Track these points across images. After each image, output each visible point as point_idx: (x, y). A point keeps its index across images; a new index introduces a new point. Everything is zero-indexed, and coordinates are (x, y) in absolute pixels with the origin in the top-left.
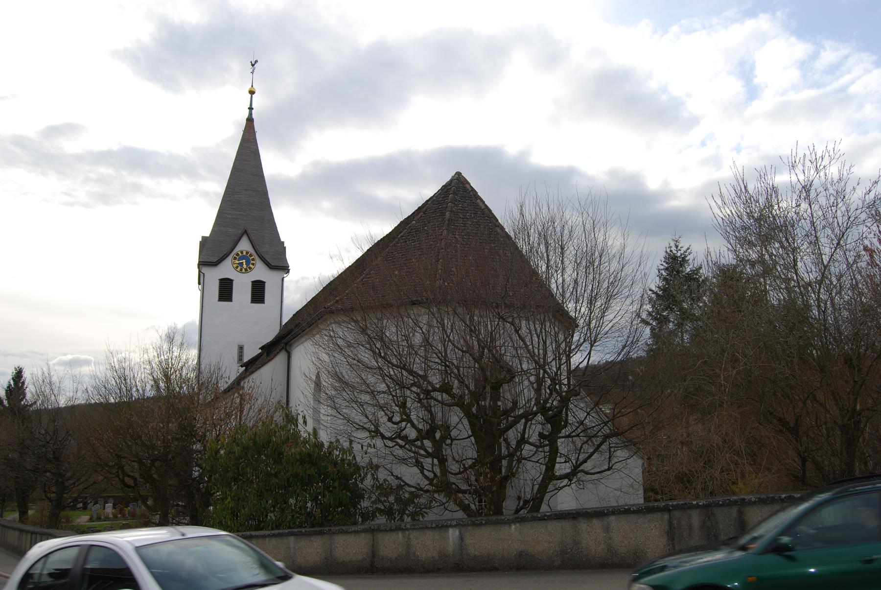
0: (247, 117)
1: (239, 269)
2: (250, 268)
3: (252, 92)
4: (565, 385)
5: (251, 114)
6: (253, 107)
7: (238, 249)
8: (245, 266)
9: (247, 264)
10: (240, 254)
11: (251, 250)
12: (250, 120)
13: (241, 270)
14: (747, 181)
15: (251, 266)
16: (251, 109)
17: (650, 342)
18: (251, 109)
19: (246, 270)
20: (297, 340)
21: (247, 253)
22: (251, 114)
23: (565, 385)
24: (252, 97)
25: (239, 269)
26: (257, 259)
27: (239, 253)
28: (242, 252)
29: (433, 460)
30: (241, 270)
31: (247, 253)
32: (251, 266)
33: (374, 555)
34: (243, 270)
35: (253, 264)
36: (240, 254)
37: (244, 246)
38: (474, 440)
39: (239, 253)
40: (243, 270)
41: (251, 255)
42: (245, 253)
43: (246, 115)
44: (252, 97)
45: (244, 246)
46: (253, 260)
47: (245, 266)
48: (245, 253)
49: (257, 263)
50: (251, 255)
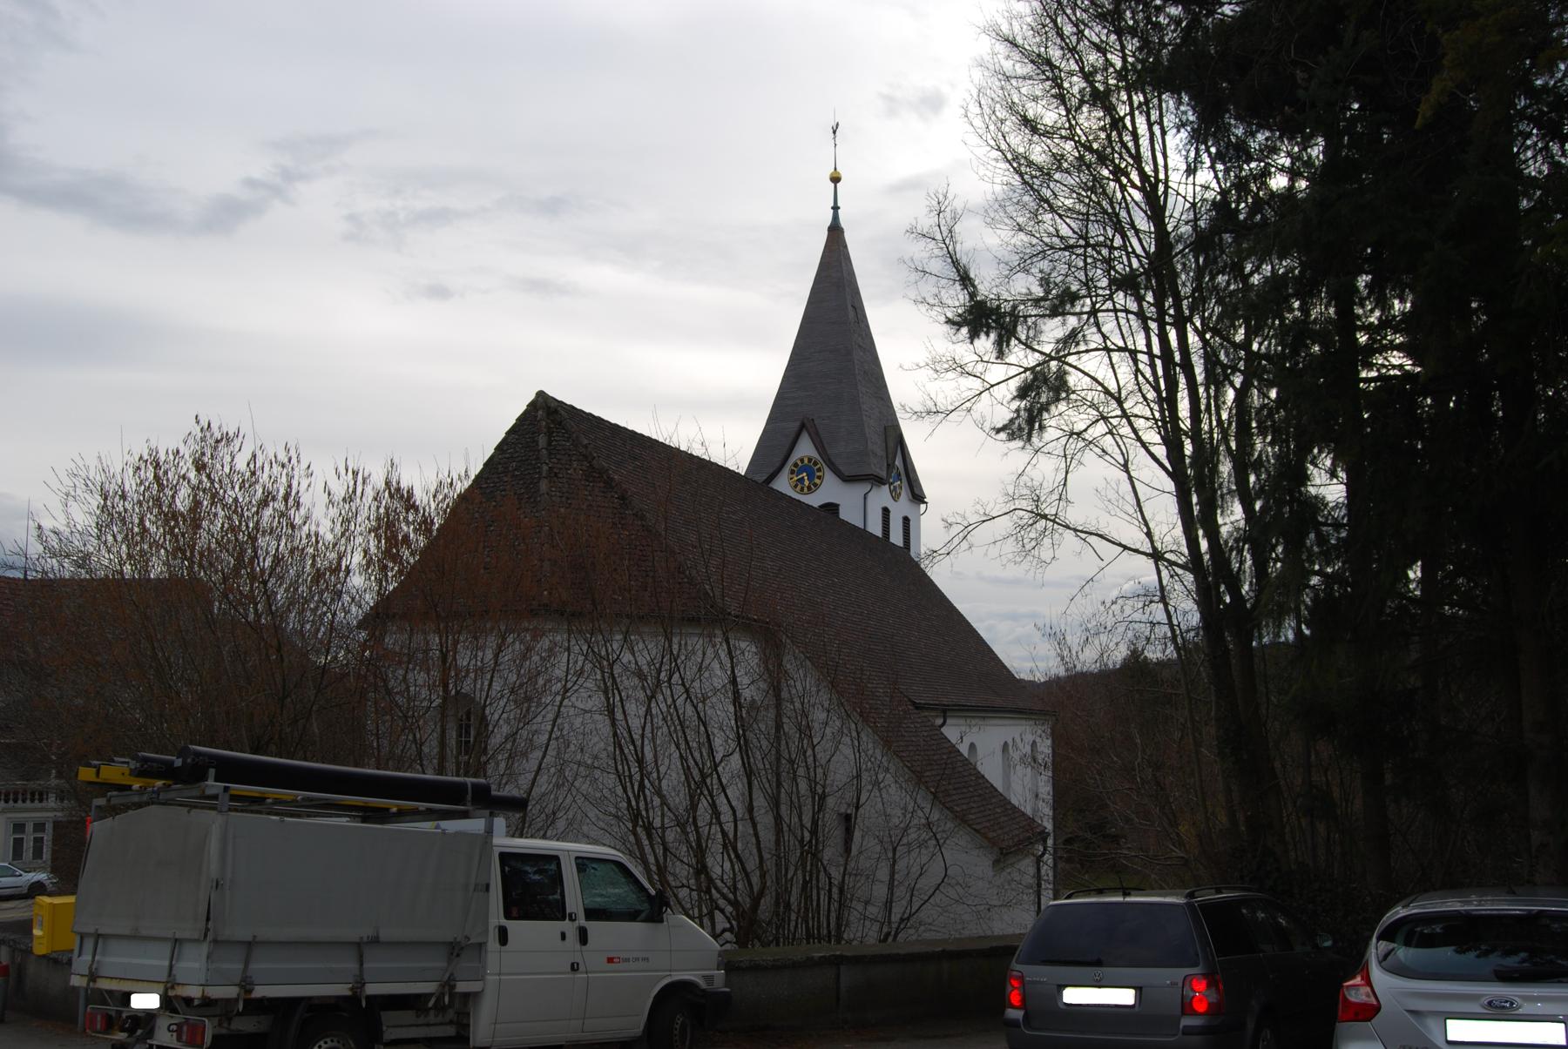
0: (829, 224)
1: (799, 487)
2: (815, 485)
3: (836, 179)
5: (836, 217)
7: (795, 457)
8: (807, 483)
10: (818, 474)
11: (814, 454)
12: (835, 231)
13: (802, 489)
14: (301, 451)
15: (817, 481)
16: (836, 208)
17: (1242, 524)
18: (836, 208)
19: (809, 488)
21: (810, 460)
22: (836, 217)
24: (836, 187)
25: (799, 487)
26: (826, 469)
27: (799, 462)
28: (802, 460)
30: (802, 489)
32: (817, 481)
33: (1203, 975)
34: (806, 489)
35: (819, 477)
36: (818, 474)
37: (805, 449)
39: (799, 462)
40: (806, 489)
41: (816, 463)
42: (806, 461)
44: (836, 187)
45: (805, 449)
46: (819, 470)
47: (807, 483)
48: (806, 461)
49: (826, 473)
50: (816, 463)
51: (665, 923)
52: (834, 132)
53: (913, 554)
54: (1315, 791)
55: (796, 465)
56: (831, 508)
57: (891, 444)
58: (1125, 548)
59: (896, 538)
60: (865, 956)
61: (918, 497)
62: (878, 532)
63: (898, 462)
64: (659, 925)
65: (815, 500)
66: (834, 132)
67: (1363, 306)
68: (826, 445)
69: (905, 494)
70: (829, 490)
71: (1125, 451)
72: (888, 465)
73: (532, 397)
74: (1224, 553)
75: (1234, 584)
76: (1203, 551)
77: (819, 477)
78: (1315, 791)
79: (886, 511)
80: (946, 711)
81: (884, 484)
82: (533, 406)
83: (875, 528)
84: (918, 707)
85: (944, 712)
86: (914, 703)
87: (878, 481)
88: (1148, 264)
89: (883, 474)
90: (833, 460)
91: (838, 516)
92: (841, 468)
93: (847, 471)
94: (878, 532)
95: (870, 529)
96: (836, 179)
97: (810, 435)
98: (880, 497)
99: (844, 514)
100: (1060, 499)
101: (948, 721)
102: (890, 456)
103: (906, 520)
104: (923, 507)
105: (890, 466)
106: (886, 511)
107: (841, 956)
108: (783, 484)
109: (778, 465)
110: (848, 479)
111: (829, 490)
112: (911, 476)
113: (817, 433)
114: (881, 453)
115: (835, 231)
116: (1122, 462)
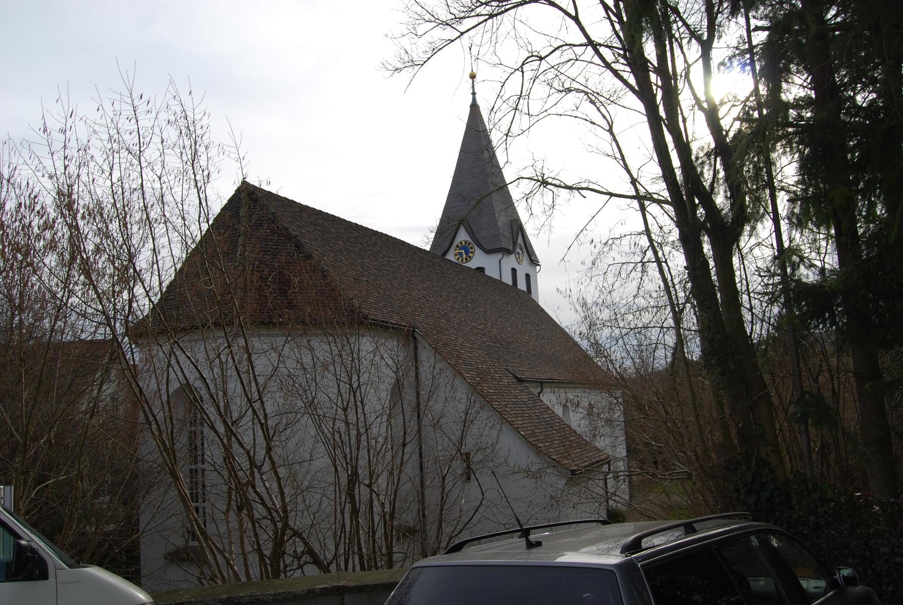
0: (470, 103)
2: (470, 257)
3: (473, 77)
4: (278, 521)
5: (474, 99)
6: (476, 91)
8: (464, 256)
9: (467, 253)
10: (471, 250)
11: (469, 239)
12: (474, 107)
15: (471, 255)
16: (474, 94)
18: (474, 94)
19: (466, 259)
20: (574, 388)
21: (466, 242)
22: (474, 99)
23: (278, 521)
26: (476, 247)
28: (461, 243)
29: (288, 571)
31: (466, 242)
32: (471, 255)
34: (464, 260)
35: (472, 252)
36: (471, 250)
37: (463, 236)
38: (734, 259)
39: (459, 244)
40: (464, 260)
41: (469, 244)
42: (464, 244)
43: (470, 102)
44: (473, 82)
45: (463, 236)
46: (471, 248)
47: (464, 256)
48: (464, 244)
50: (469, 244)
51: (52, 579)
52: (470, 49)
53: (533, 296)
54: (807, 396)
55: (458, 246)
56: (481, 270)
57: (515, 230)
58: (612, 195)
59: (522, 285)
60: (367, 586)
61: (534, 261)
62: (510, 283)
63: (520, 241)
64: (41, 584)
65: (473, 264)
66: (470, 49)
67: (800, 117)
68: (475, 234)
69: (525, 259)
70: (478, 259)
71: (610, 120)
72: (514, 243)
73: (238, 184)
74: (694, 168)
75: (707, 198)
76: (674, 166)
77: (472, 252)
78: (807, 396)
79: (514, 271)
80: (542, 384)
81: (512, 254)
82: (238, 191)
83: (508, 280)
84: (520, 380)
85: (541, 383)
86: (517, 378)
87: (509, 252)
88: (641, 22)
89: (511, 248)
90: (479, 241)
91: (484, 273)
92: (484, 245)
93: (488, 248)
94: (510, 283)
95: (504, 280)
96: (473, 77)
97: (465, 227)
98: (510, 262)
99: (488, 272)
100: (516, 109)
101: (544, 390)
102: (514, 237)
103: (528, 276)
104: (538, 268)
105: (515, 243)
106: (514, 271)
107: (343, 587)
108: (451, 256)
109: (447, 247)
110: (489, 252)
111: (478, 259)
112: (529, 249)
113: (470, 227)
114: (508, 235)
115: (474, 107)
116: (607, 128)
